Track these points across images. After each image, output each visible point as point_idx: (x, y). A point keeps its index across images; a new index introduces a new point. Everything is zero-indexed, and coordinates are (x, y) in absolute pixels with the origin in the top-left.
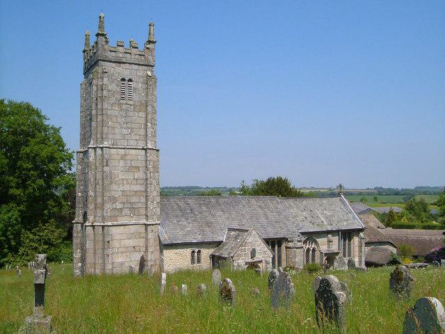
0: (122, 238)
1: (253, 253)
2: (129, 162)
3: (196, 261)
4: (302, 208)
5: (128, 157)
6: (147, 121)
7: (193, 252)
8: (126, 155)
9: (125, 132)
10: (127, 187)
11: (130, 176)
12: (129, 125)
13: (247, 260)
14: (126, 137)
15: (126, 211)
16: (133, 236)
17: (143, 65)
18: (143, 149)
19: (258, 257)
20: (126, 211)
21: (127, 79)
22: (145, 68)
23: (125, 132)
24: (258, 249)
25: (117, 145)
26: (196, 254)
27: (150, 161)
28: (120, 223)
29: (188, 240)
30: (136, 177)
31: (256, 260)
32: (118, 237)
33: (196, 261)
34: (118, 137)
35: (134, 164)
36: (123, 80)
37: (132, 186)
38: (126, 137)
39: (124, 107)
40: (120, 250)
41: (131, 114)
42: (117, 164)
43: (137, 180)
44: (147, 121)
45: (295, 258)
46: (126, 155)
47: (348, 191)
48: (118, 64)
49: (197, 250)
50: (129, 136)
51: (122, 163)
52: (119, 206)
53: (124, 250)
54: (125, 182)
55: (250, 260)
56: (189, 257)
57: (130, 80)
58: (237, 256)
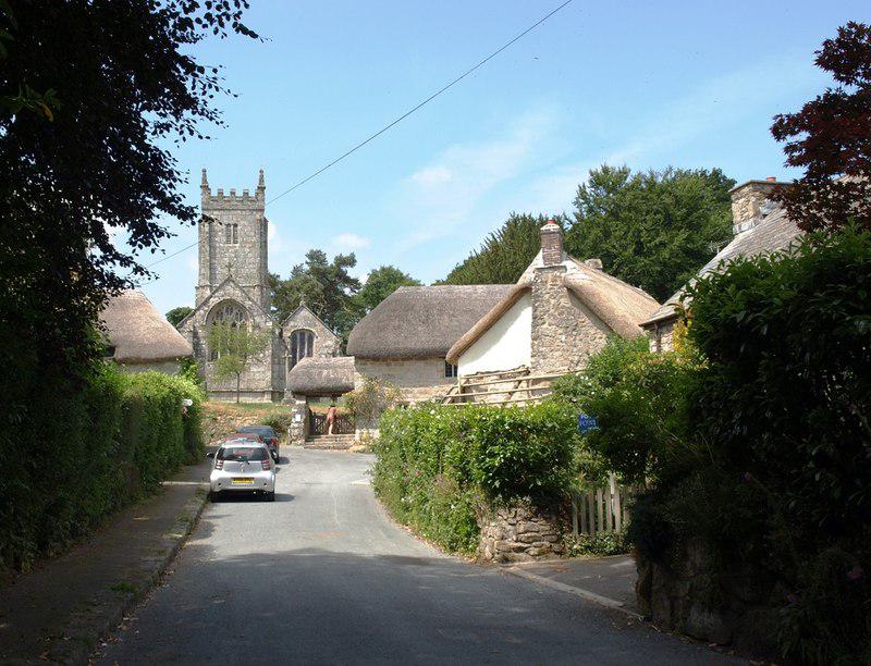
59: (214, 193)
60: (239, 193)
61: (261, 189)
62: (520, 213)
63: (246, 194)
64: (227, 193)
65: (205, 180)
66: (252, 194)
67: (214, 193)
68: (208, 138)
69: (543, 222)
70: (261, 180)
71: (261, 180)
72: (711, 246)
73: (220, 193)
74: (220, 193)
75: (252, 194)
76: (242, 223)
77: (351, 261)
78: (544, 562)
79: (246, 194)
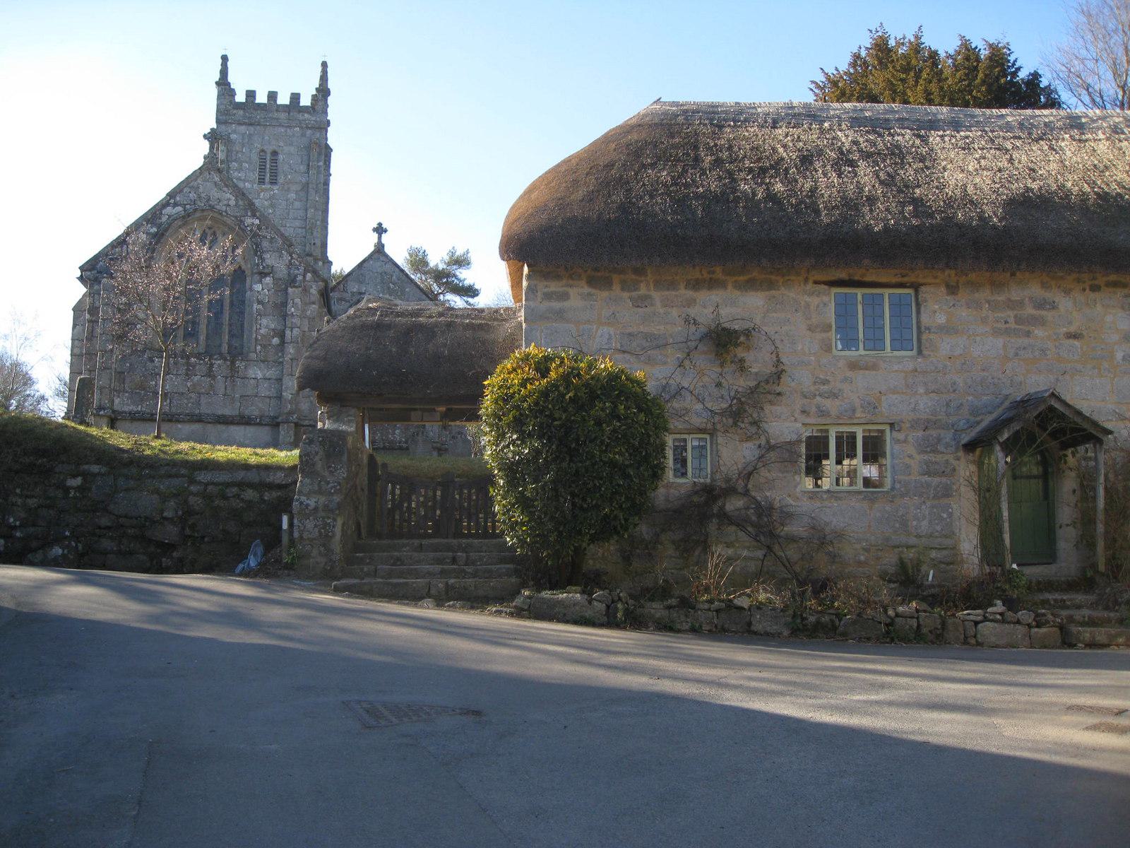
59: (240, 97)
60: (284, 99)
61: (323, 92)
62: (900, 31)
63: (295, 97)
64: (261, 98)
65: (224, 72)
66: (306, 101)
67: (240, 97)
68: (380, 230)
69: (460, 608)
70: (324, 78)
71: (324, 78)
72: (684, 454)
73: (251, 94)
74: (251, 94)
75: (306, 101)
76: (286, 149)
77: (461, 262)
78: (546, 304)
79: (295, 97)
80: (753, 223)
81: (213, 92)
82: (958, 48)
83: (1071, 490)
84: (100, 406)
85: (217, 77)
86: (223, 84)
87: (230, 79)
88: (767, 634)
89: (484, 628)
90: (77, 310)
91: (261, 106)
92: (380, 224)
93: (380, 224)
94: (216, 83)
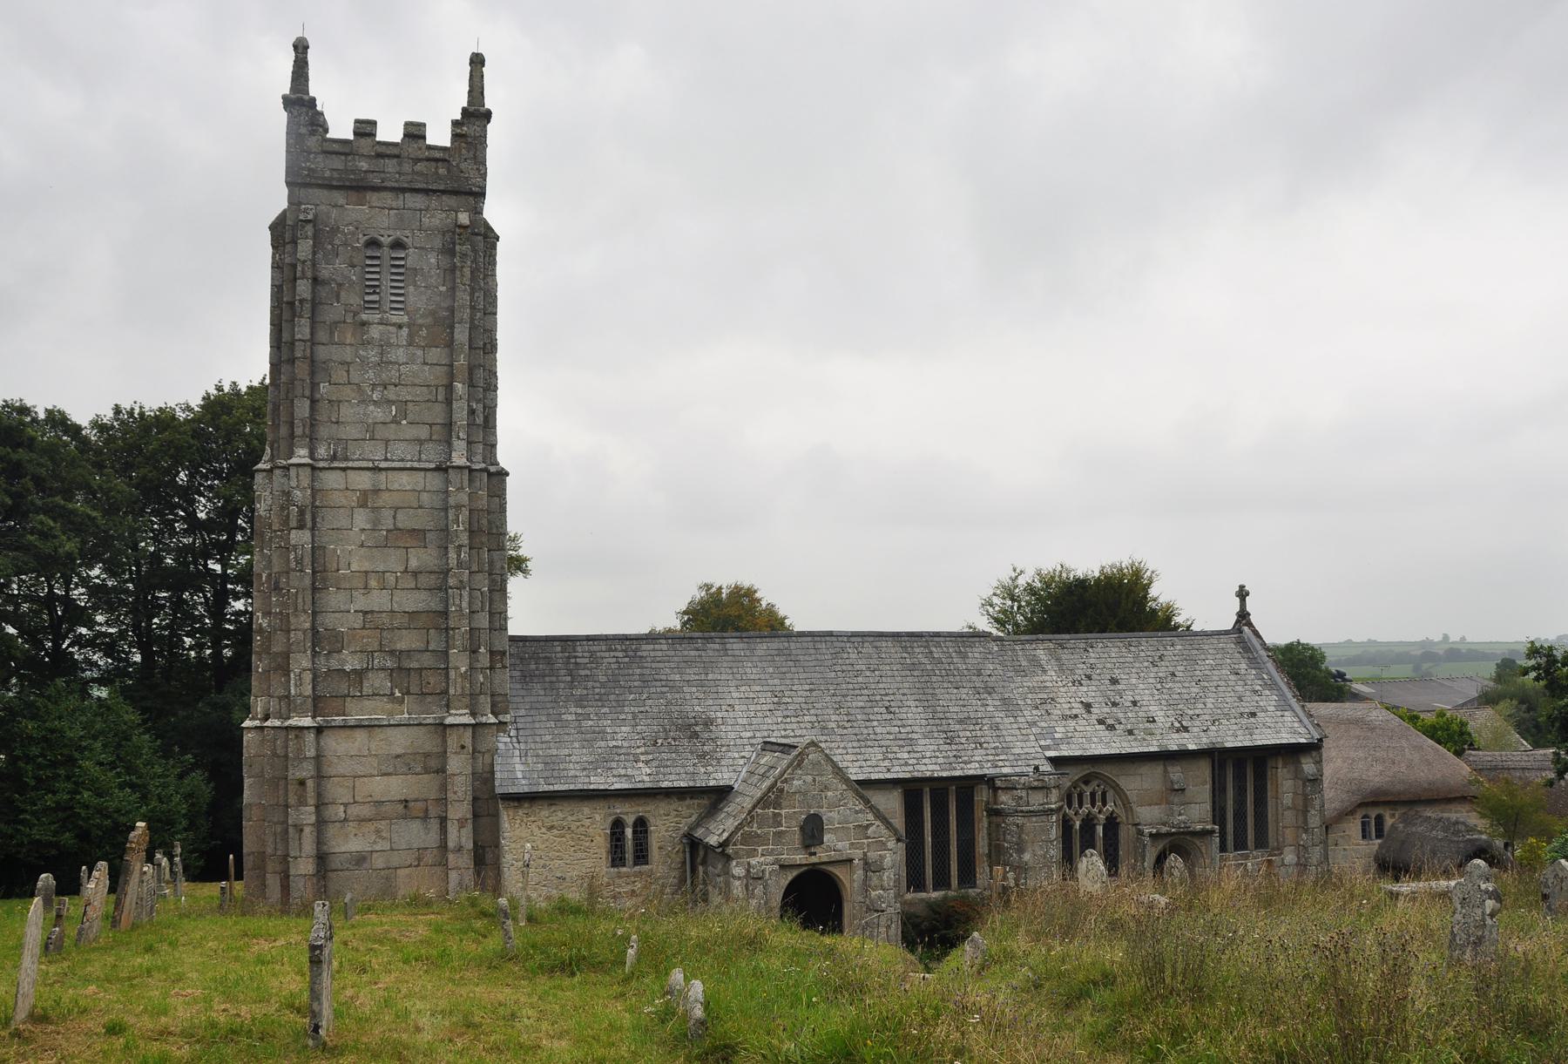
0: (360, 770)
1: (812, 830)
2: (387, 515)
3: (629, 856)
4: (1081, 670)
5: (386, 498)
6: (452, 377)
7: (618, 825)
8: (377, 491)
9: (377, 414)
10: (378, 600)
11: (392, 562)
12: (391, 394)
13: (786, 857)
14: (381, 432)
15: (378, 681)
16: (401, 763)
17: (444, 192)
18: (437, 469)
19: (835, 844)
20: (378, 681)
21: (386, 240)
22: (451, 201)
23: (377, 414)
24: (831, 817)
25: (346, 459)
26: (629, 832)
27: (459, 507)
28: (352, 719)
29: (598, 782)
30: (414, 563)
31: (822, 855)
32: (343, 767)
33: (629, 856)
34: (352, 432)
35: (404, 520)
36: (373, 243)
37: (398, 596)
38: (381, 432)
39: (375, 332)
40: (354, 811)
41: (400, 354)
42: (344, 523)
43: (415, 574)
44: (452, 377)
45: (1021, 851)
46: (377, 491)
47: (1473, 647)
48: (353, 195)
49: (630, 820)
50: (392, 430)
51: (361, 519)
52: (351, 663)
53: (366, 811)
54: (373, 583)
55: (800, 858)
56: (601, 844)
57: (398, 245)
58: (744, 841)
59: (340, 128)
63: (415, 132)
66: (439, 136)
73: (365, 129)
75: (439, 136)
80: (174, 745)
81: (279, 119)
82: (1178, 619)
83: (964, 956)
84: (321, 303)
85: (283, 84)
86: (300, 104)
87: (314, 90)
88: (870, 636)
89: (1386, 793)
90: (1350, 641)
91: (387, 152)
92: (1242, 587)
93: (1242, 587)
94: (285, 98)
